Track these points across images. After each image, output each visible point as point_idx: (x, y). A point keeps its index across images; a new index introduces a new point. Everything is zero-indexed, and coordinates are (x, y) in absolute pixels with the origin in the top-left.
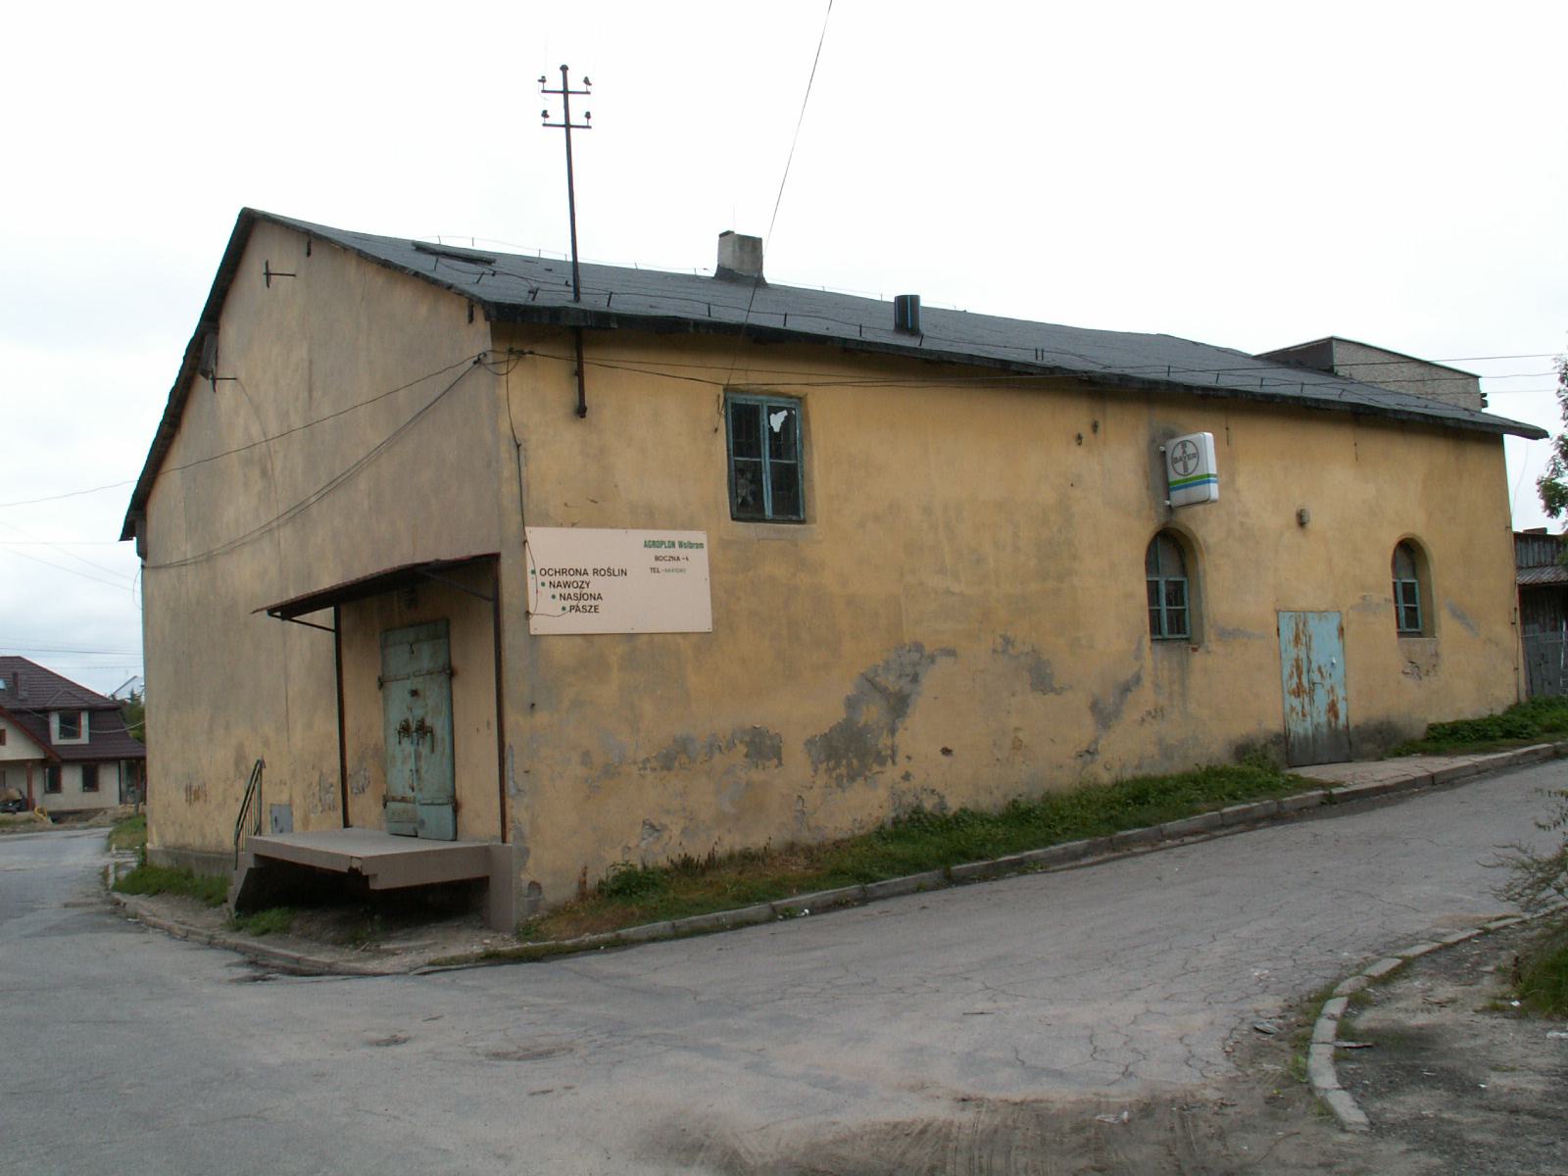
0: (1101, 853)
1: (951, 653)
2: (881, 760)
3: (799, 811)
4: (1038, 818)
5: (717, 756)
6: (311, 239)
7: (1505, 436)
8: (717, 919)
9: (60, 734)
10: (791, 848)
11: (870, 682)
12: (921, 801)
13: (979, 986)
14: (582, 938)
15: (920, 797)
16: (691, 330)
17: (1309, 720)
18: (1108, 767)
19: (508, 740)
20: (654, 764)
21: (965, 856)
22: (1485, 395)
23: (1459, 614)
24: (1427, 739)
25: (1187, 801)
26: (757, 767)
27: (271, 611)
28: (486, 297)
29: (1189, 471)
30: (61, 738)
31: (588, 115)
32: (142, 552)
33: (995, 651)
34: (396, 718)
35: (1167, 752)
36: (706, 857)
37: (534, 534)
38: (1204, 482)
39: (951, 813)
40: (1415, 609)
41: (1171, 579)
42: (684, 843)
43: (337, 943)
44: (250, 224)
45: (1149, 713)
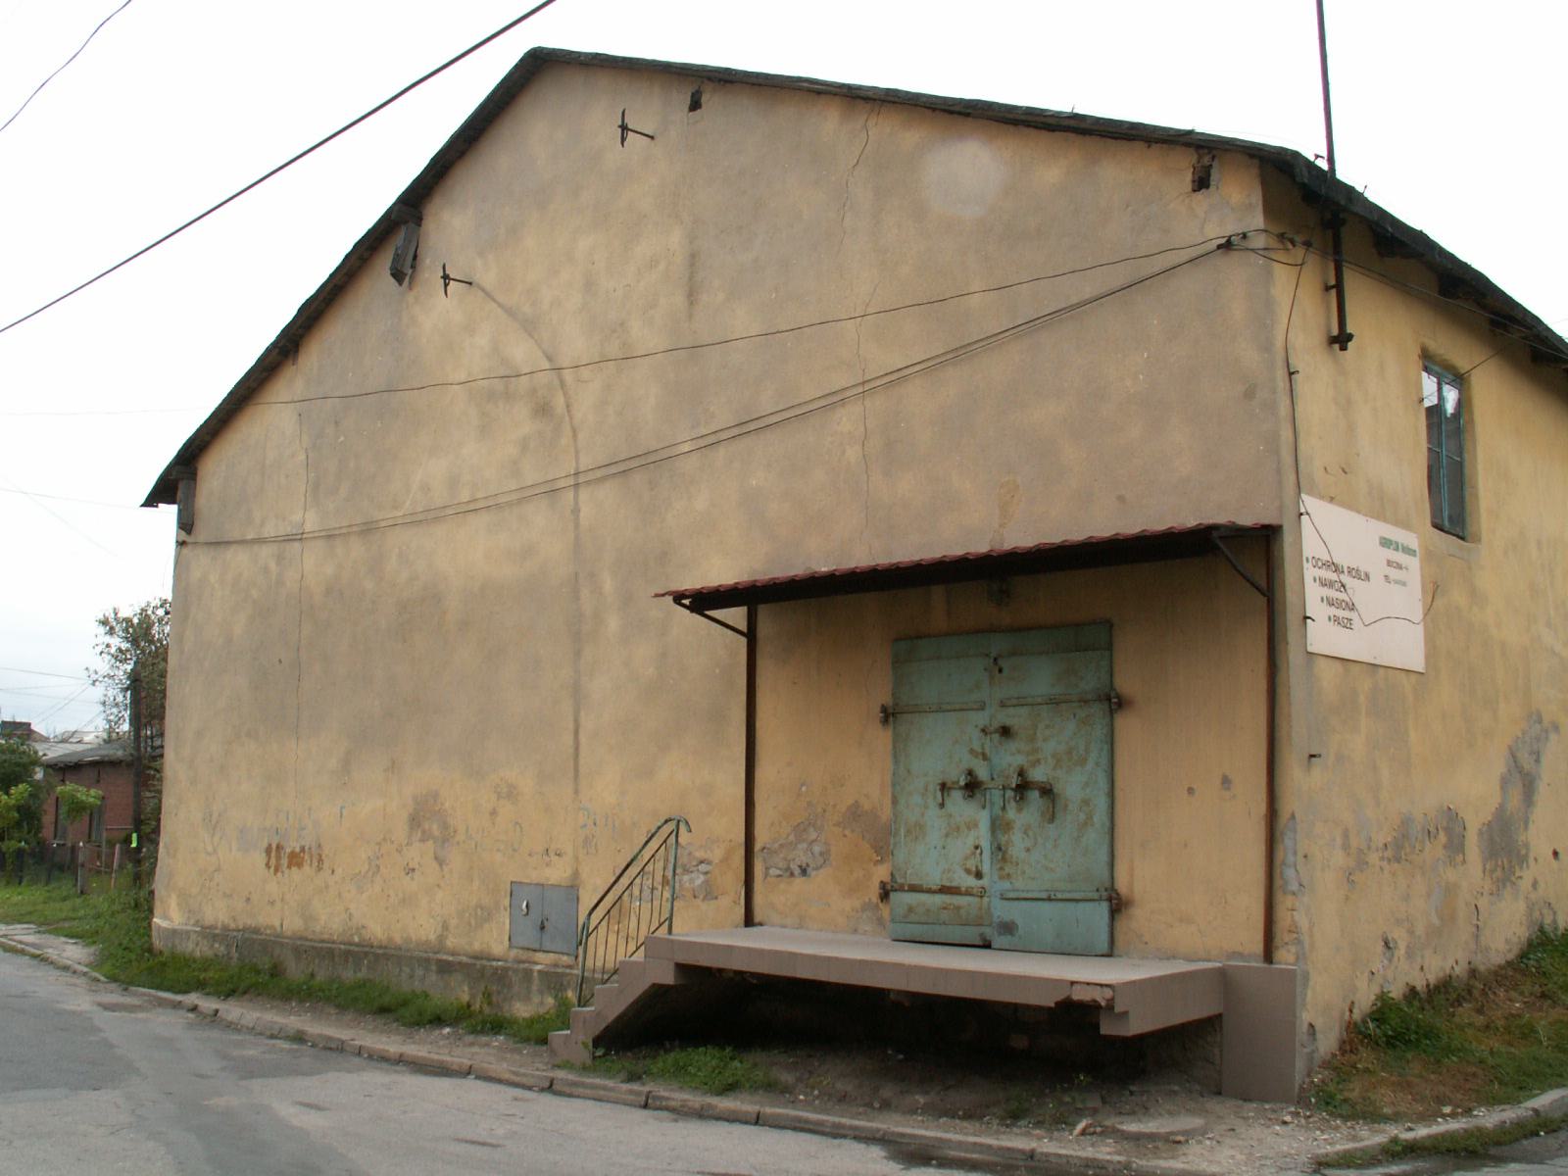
27: (678, 597)
32: (186, 524)
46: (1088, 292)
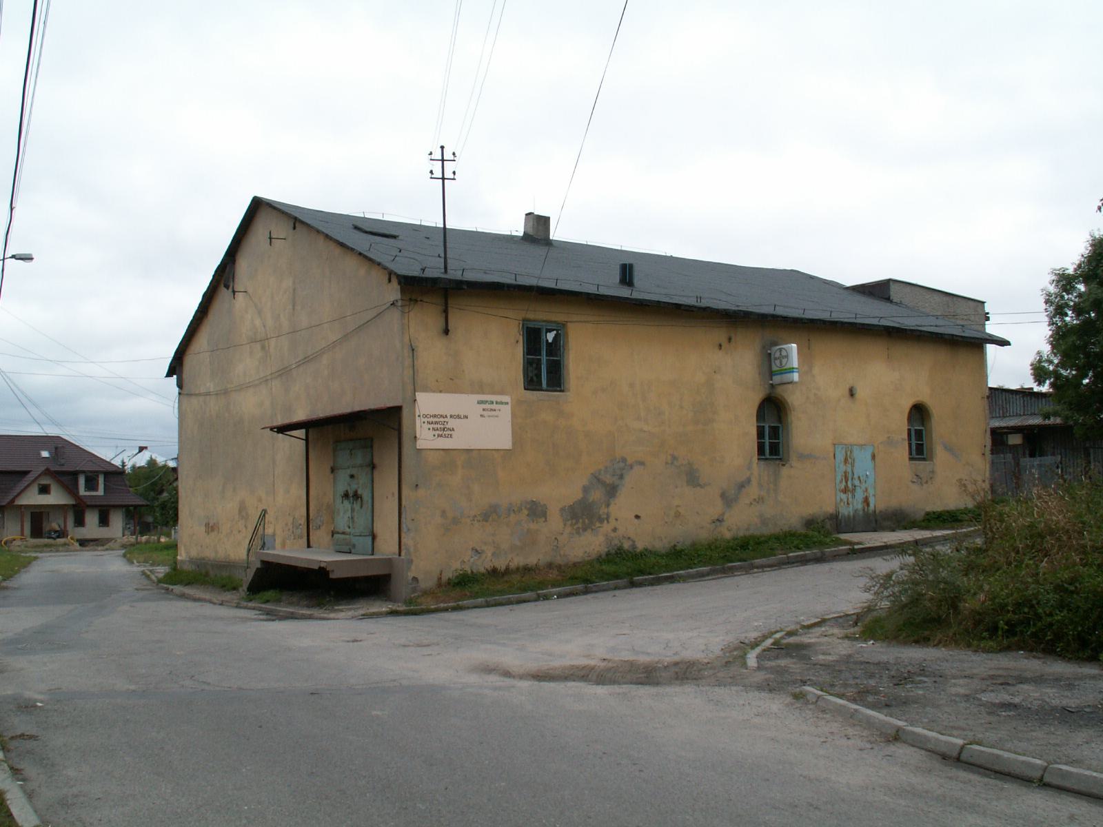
0: (717, 574)
1: (642, 463)
2: (601, 520)
3: (555, 546)
4: (686, 555)
5: (512, 515)
6: (297, 221)
7: (988, 345)
8: (509, 598)
9: (86, 488)
10: (550, 566)
11: (597, 479)
12: (622, 544)
13: (627, 625)
14: (439, 605)
15: (622, 541)
16: (506, 289)
17: (852, 506)
18: (729, 528)
19: (404, 503)
20: (479, 518)
21: (642, 572)
22: (988, 313)
23: (949, 449)
24: (923, 521)
25: (771, 549)
26: (533, 522)
27: (272, 429)
28: (399, 272)
29: (784, 364)
30: (85, 491)
31: (454, 173)
33: (667, 463)
34: (341, 489)
35: (764, 522)
36: (505, 568)
37: (420, 396)
38: (790, 372)
39: (638, 551)
40: (922, 444)
41: (773, 425)
42: (493, 560)
43: (308, 607)
44: (257, 205)
45: (755, 500)
46: (369, 317)
